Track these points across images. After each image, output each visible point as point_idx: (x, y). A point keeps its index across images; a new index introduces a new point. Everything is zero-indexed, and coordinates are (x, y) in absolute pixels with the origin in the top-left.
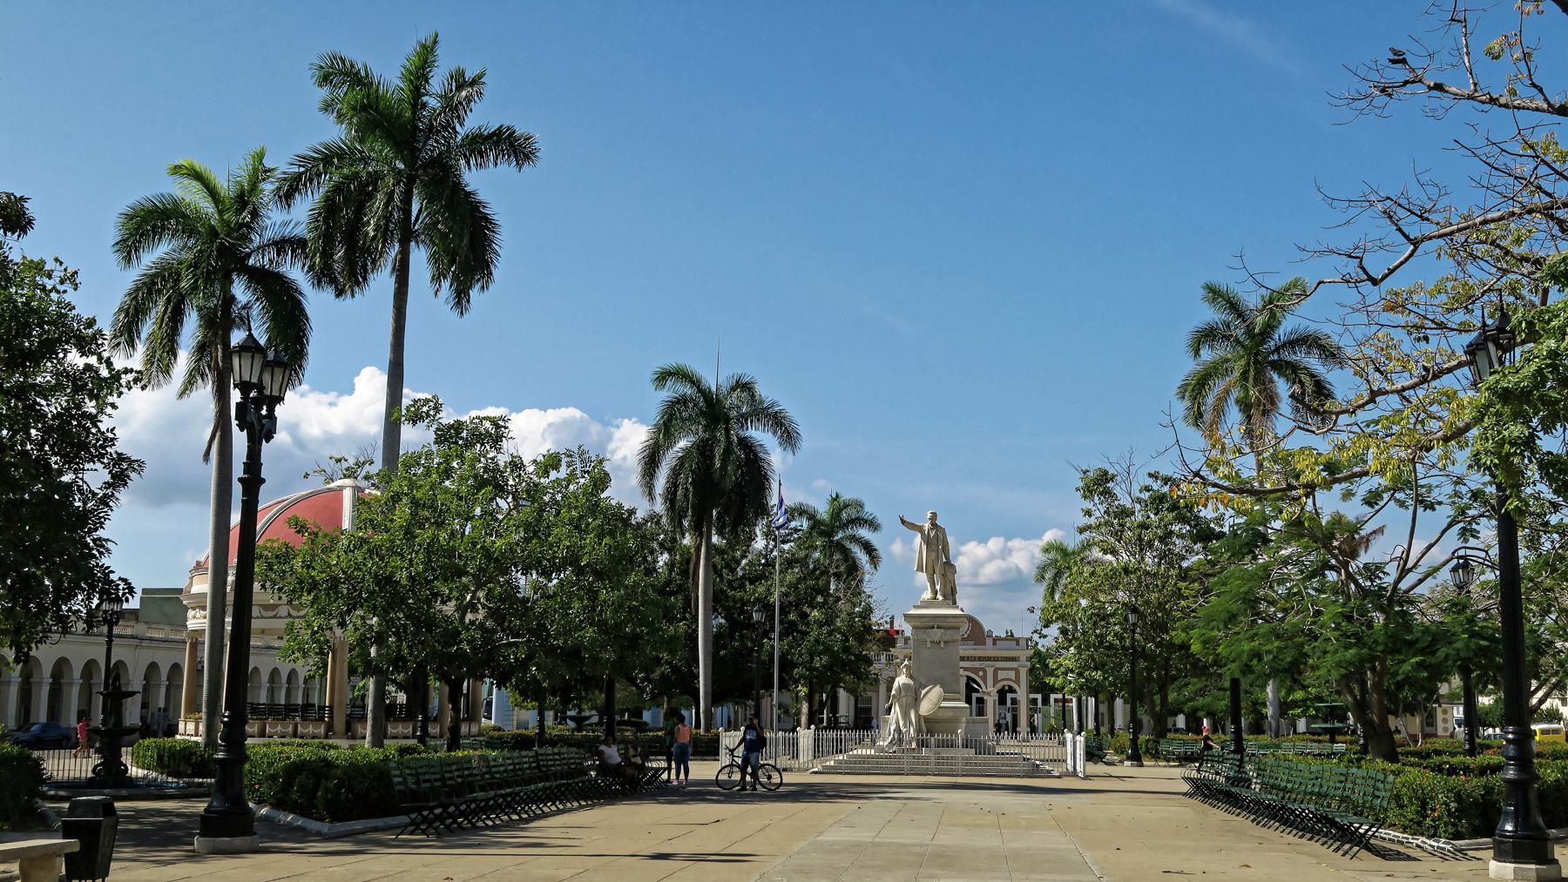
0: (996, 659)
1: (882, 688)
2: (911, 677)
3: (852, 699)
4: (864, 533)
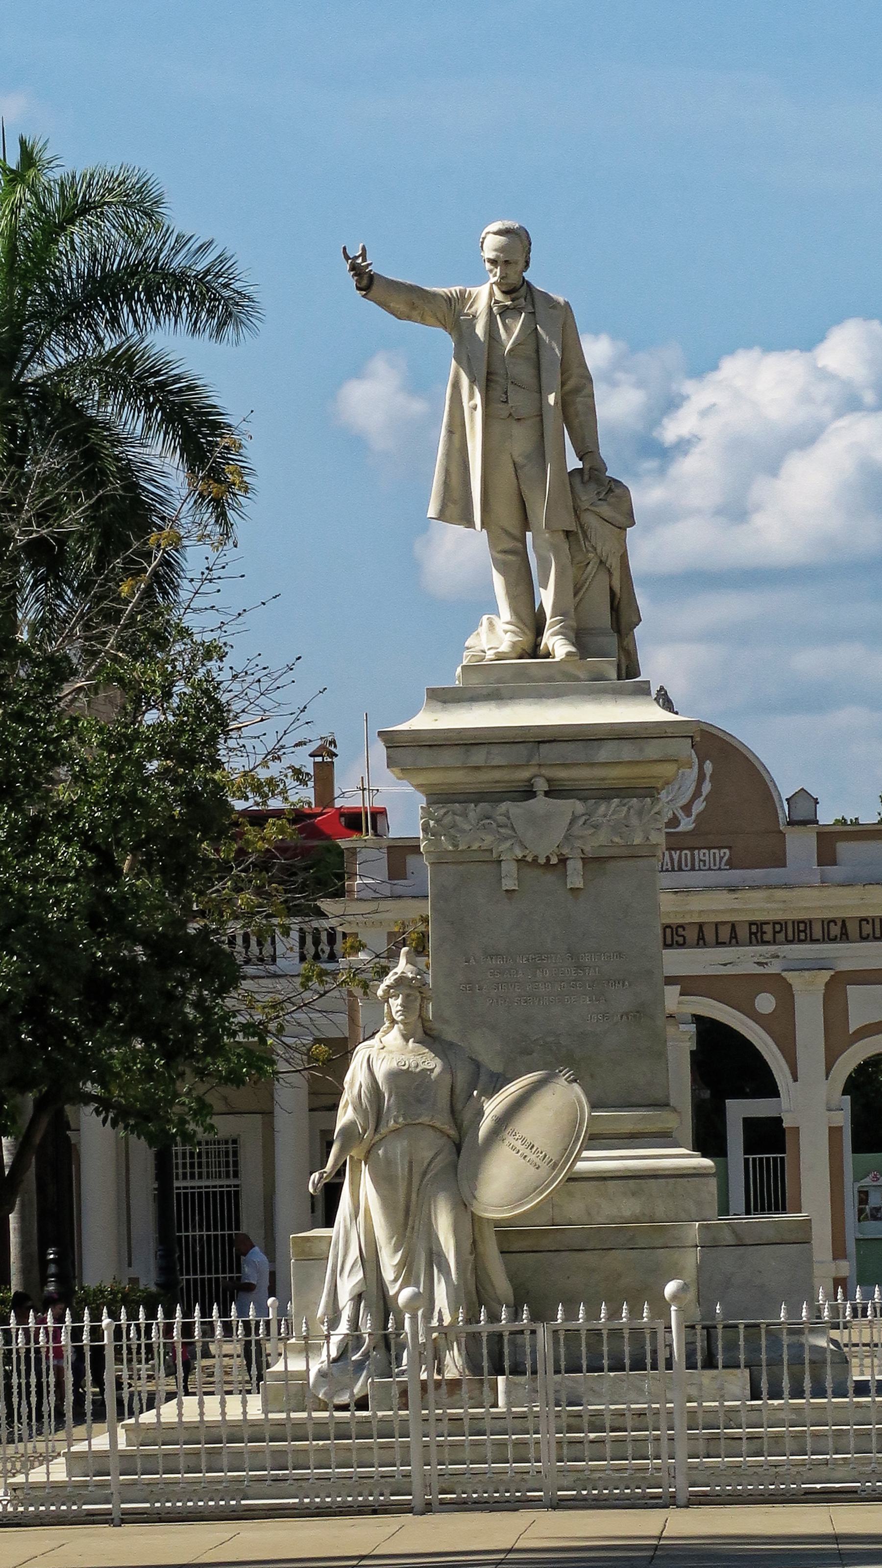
0: (839, 931)
1: (290, 1094)
2: (426, 1035)
3: (143, 1154)
4: (172, 343)
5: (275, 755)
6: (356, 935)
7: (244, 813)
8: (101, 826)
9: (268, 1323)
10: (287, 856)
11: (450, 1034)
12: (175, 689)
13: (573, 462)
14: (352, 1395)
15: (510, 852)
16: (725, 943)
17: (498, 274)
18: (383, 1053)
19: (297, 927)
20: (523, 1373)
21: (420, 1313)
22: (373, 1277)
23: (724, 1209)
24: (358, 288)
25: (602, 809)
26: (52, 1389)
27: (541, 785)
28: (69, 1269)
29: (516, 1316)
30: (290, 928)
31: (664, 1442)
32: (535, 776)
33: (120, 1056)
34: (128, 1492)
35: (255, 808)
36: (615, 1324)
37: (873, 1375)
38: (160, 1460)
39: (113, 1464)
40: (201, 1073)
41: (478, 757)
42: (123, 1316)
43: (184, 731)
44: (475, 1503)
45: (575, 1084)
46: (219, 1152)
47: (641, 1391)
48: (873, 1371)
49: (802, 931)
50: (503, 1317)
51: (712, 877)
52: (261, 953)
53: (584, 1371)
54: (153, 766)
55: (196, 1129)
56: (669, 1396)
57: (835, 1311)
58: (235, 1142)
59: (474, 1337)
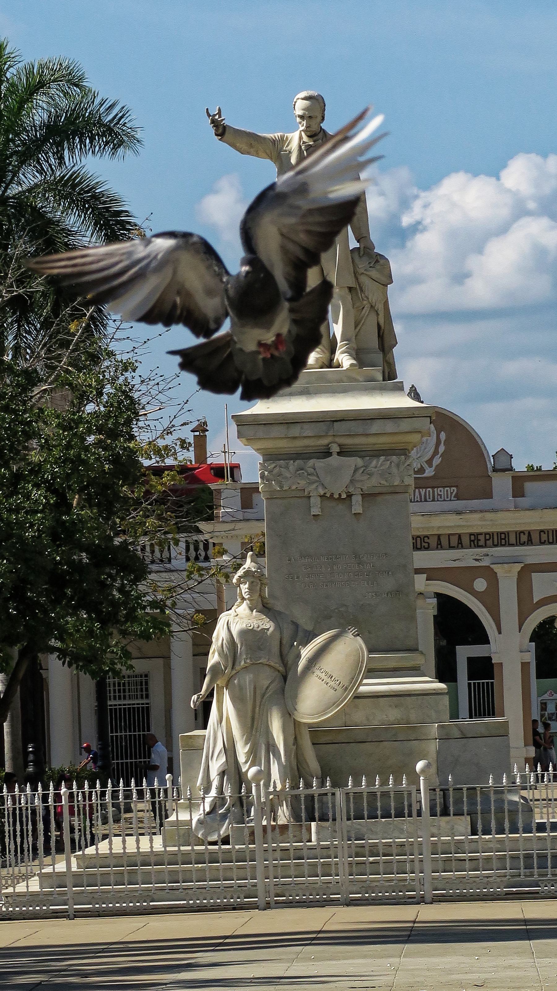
0: (526, 538)
1: (181, 645)
2: (264, 607)
3: (88, 684)
4: (94, 165)
5: (168, 431)
6: (221, 544)
7: (149, 468)
8: (59, 477)
9: (166, 791)
10: (177, 494)
11: (279, 606)
12: (105, 390)
13: (353, 244)
14: (219, 835)
15: (315, 491)
16: (454, 547)
17: (305, 125)
18: (237, 619)
19: (184, 540)
20: (328, 820)
21: (262, 783)
22: (232, 761)
23: (454, 715)
24: (216, 135)
25: (374, 463)
26: (30, 833)
27: (335, 449)
28: (42, 756)
29: (322, 784)
30: (179, 541)
31: (417, 863)
32: (331, 443)
33: (73, 622)
34: (78, 898)
35: (156, 465)
36: (385, 789)
37: (548, 819)
38: (99, 877)
39: (69, 881)
40: (124, 633)
41: (295, 431)
42: (75, 787)
43: (111, 417)
44: (298, 902)
45: (358, 637)
46: (136, 682)
47: (402, 831)
48: (548, 816)
49: (503, 539)
50: (314, 785)
51: (447, 505)
52: (161, 556)
53: (366, 818)
54: (91, 439)
55: (122, 668)
56: (420, 833)
57: (524, 778)
58: (146, 676)
59: (296, 798)
